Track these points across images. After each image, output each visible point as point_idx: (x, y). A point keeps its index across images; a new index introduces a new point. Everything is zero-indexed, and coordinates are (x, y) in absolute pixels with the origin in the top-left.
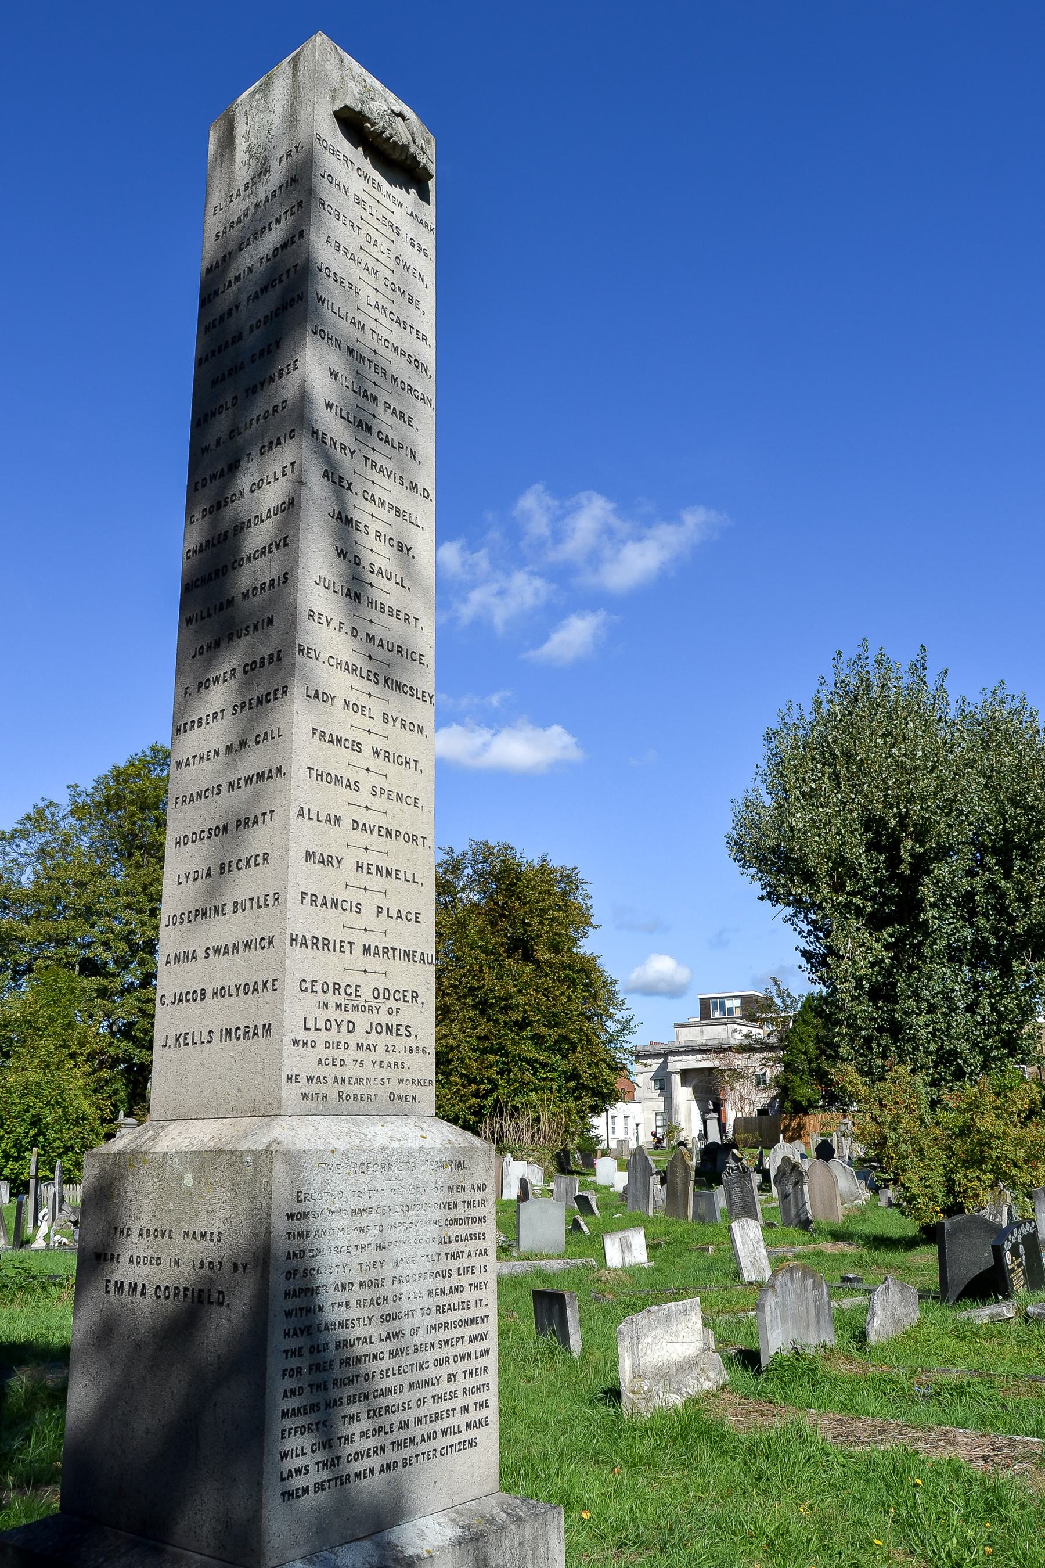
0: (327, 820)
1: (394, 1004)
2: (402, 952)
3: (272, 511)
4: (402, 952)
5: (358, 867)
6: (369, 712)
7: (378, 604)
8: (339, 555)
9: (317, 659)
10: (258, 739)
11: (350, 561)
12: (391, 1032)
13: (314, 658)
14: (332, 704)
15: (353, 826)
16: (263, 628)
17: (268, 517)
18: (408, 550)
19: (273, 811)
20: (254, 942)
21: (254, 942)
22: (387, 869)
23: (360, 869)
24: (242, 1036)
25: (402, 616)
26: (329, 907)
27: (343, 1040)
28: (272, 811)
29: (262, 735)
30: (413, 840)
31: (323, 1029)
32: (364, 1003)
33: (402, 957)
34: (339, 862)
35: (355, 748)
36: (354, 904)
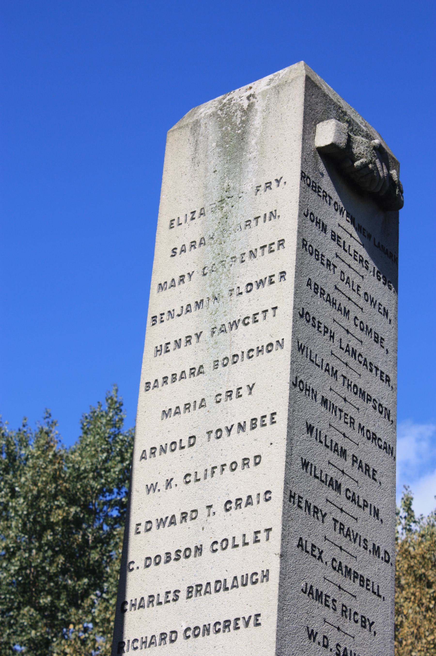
3: (239, 579)
8: (310, 637)
11: (319, 643)
17: (233, 587)
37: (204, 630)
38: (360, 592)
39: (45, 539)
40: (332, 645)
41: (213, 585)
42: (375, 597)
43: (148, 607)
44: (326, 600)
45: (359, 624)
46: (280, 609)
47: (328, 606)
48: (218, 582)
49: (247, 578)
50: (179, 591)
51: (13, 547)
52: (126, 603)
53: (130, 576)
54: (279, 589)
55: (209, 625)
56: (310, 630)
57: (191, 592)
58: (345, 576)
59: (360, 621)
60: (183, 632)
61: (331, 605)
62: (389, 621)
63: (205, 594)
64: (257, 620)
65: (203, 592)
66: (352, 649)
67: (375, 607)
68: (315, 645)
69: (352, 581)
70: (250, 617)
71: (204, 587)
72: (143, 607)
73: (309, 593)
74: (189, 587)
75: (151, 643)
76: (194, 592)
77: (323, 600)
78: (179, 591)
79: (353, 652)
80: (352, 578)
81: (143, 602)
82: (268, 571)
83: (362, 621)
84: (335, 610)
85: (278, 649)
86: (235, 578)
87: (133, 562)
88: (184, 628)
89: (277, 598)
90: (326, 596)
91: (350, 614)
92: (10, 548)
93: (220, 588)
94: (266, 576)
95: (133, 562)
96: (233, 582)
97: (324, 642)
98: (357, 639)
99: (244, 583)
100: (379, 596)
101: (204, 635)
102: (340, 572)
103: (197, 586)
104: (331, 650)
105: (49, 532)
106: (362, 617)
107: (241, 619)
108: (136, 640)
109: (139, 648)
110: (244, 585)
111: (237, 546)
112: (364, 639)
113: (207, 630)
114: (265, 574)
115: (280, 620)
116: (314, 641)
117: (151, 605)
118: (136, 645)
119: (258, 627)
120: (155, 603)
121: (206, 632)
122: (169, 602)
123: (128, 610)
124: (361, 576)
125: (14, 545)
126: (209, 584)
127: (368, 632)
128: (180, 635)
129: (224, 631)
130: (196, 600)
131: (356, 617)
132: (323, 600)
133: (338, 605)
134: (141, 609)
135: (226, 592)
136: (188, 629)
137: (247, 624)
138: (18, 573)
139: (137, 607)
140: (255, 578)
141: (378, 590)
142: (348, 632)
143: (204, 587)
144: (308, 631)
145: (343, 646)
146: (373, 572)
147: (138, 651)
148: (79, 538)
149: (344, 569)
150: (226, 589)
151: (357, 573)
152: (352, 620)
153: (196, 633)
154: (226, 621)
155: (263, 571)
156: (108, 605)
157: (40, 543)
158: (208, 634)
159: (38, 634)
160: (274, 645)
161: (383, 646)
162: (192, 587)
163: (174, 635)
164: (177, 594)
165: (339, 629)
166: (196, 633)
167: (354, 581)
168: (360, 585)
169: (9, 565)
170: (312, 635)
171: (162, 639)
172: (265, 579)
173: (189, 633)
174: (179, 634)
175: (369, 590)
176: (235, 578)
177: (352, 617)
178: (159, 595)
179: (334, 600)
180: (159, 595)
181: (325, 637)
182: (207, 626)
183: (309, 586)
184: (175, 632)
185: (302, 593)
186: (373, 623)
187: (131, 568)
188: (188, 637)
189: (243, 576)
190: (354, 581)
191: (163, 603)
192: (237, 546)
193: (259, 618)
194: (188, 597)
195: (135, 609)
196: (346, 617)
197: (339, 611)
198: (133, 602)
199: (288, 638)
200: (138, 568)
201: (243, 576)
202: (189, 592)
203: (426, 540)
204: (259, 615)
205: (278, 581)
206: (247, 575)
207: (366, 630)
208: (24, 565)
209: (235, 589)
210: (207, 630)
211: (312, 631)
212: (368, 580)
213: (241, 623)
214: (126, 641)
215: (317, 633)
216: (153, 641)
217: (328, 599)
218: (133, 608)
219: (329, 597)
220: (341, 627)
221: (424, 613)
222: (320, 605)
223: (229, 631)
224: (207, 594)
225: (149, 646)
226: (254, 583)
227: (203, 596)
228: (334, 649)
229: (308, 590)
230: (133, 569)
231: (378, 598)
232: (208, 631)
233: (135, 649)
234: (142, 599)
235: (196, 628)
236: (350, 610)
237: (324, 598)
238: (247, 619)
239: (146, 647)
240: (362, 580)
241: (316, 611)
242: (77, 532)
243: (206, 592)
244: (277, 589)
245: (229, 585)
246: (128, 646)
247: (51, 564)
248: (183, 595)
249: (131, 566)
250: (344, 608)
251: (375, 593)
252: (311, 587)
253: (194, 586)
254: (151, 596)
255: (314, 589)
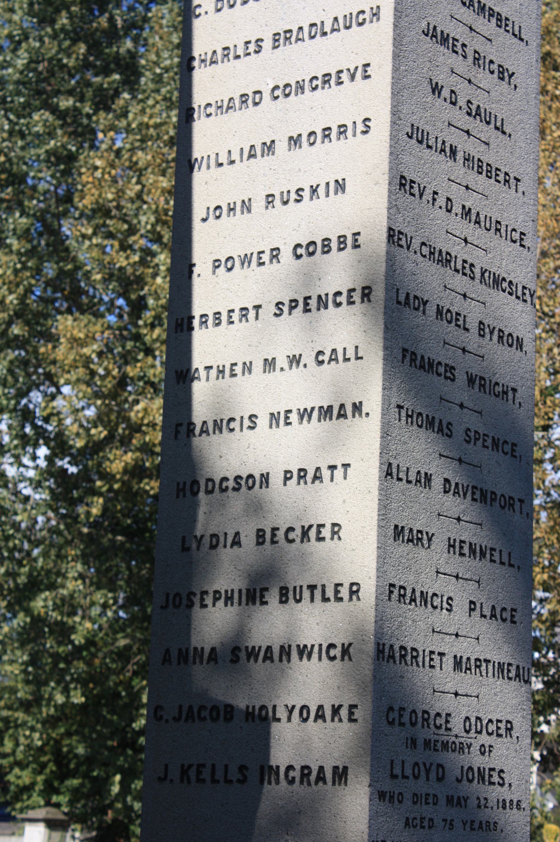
0: (417, 481)
1: (484, 739)
2: (496, 664)
3: (341, 21)
4: (496, 664)
5: (450, 546)
6: (464, 321)
7: (476, 160)
8: (433, 92)
9: (408, 248)
10: (321, 358)
11: (445, 100)
12: (483, 780)
13: (405, 246)
14: (424, 313)
15: (445, 487)
16: (327, 195)
17: (333, 30)
18: (511, 76)
19: (349, 465)
20: (316, 649)
21: (316, 649)
22: (481, 546)
23: (452, 549)
24: (298, 779)
25: (501, 178)
26: (418, 604)
27: (432, 792)
28: (346, 466)
29: (328, 353)
30: (510, 504)
31: (411, 777)
32: (453, 739)
33: (496, 674)
34: (430, 540)
35: (448, 374)
36: (445, 599)
37: (297, 88)
38: (498, 35)
39: (60, 22)
40: (462, 102)
41: (306, 30)
42: (515, 40)
43: (223, 62)
44: (454, 45)
45: (496, 75)
46: (396, 56)
47: (456, 53)
48: (313, 25)
49: (351, 18)
50: (262, 40)
51: (19, 35)
52: (193, 58)
53: (197, 24)
54: (394, 31)
55: (303, 81)
56: (434, 83)
57: (277, 40)
58: (478, 14)
59: (496, 71)
60: (269, 91)
61: (460, 51)
62: (533, 72)
63: (296, 42)
64: (366, 71)
65: (293, 39)
66: (487, 107)
67: (516, 53)
68: (441, 100)
69: (486, 20)
70: (357, 68)
71: (295, 33)
72: (215, 62)
73: (433, 36)
74: (275, 35)
75: (229, 108)
76: (282, 41)
77: (450, 45)
78: (262, 40)
79: (488, 110)
80: (487, 17)
81: (215, 57)
82: (378, 7)
83: (499, 72)
84: (465, 57)
85: (393, 106)
86: (336, 19)
87: (199, 6)
88: (271, 86)
89: (391, 41)
90: (454, 39)
91: (484, 63)
92: (14, 36)
93: (316, 33)
94: (376, 14)
95: (199, 6)
96: (333, 25)
97: (451, 98)
98: (493, 94)
99: (348, 25)
100: (521, 39)
101: (296, 95)
102: (471, 8)
103: (286, 32)
104: (460, 108)
105: (64, 14)
106: (500, 66)
107: (345, 71)
108: (209, 105)
109: (214, 114)
110: (347, 28)
111: (221, 165)
112: (501, 94)
113: (300, 87)
114: (374, 12)
115: (395, 70)
116: (439, 97)
117: (226, 59)
118: (209, 110)
119: (367, 81)
120: (231, 56)
121: (300, 90)
122: (249, 54)
123: (197, 68)
124: (499, 14)
125: (20, 32)
126: (301, 28)
127: (507, 86)
128: (267, 96)
129: (323, 88)
130: (284, 50)
131: (492, 66)
132: (450, 45)
133: (470, 52)
134: (213, 65)
135: (324, 38)
136: (276, 87)
137: (353, 77)
138: (27, 67)
139: (208, 63)
140: (361, 17)
141: (520, 31)
142: (481, 86)
143: (295, 33)
144: (432, 84)
145: (475, 103)
146: (514, 9)
147: (212, 118)
148: (103, 21)
149: (476, 5)
150: (324, 34)
151: (492, 10)
152: (487, 71)
153: (287, 91)
154: (325, 75)
155: (372, 8)
156: (145, 106)
157: (53, 29)
158: (303, 93)
159: (59, 144)
160: (389, 102)
161: (525, 103)
162: (279, 34)
163: (258, 96)
164: (259, 43)
165: (470, 81)
166: (287, 91)
167: (489, 21)
168: (498, 25)
169: (15, 58)
170: (436, 89)
171: (243, 102)
172: (375, 18)
173: (277, 93)
174: (264, 95)
175: (508, 31)
176: (336, 19)
177: (487, 67)
178: (235, 46)
179: (464, 45)
180: (235, 46)
181: (452, 92)
182: (301, 83)
183: (431, 27)
184: (259, 92)
185: (423, 36)
186: (513, 73)
187: (197, 13)
188: (276, 98)
189: (345, 16)
190: (489, 21)
191: (242, 56)
192: (221, 165)
193: (368, 69)
194: (275, 47)
195: (206, 66)
196: (479, 67)
197: (470, 59)
198: (203, 57)
199: (406, 93)
200: (206, 13)
201: (345, 16)
202: (276, 40)
203: (552, 9)
204: (368, 65)
205: (392, 20)
206: (351, 14)
207: (504, 84)
208: (34, 58)
209: (335, 33)
210: (300, 87)
211: (437, 83)
212: (507, 19)
213: (345, 77)
214: (195, 106)
215: (442, 87)
216: (231, 105)
217: (456, 43)
218: (203, 65)
219: (457, 40)
220: (473, 80)
221: (549, 103)
222: (446, 51)
223: (330, 87)
224: (299, 42)
225: (227, 112)
226: (360, 24)
227: (294, 45)
228: (464, 106)
229: (431, 32)
230: (200, 15)
231: (520, 42)
232: (302, 88)
233: (209, 115)
234: (215, 52)
235: (287, 85)
236: (484, 57)
237: (451, 41)
238: (352, 71)
239: (222, 113)
240: (499, 20)
241: (441, 59)
242: (102, 14)
243: (298, 40)
244: (392, 30)
245: (327, 29)
246: (199, 112)
247: (69, 56)
248: (267, 44)
249: (198, 11)
250: (477, 55)
251: (515, 36)
252: (435, 28)
253: (281, 32)
254: (225, 49)
255: (439, 30)
